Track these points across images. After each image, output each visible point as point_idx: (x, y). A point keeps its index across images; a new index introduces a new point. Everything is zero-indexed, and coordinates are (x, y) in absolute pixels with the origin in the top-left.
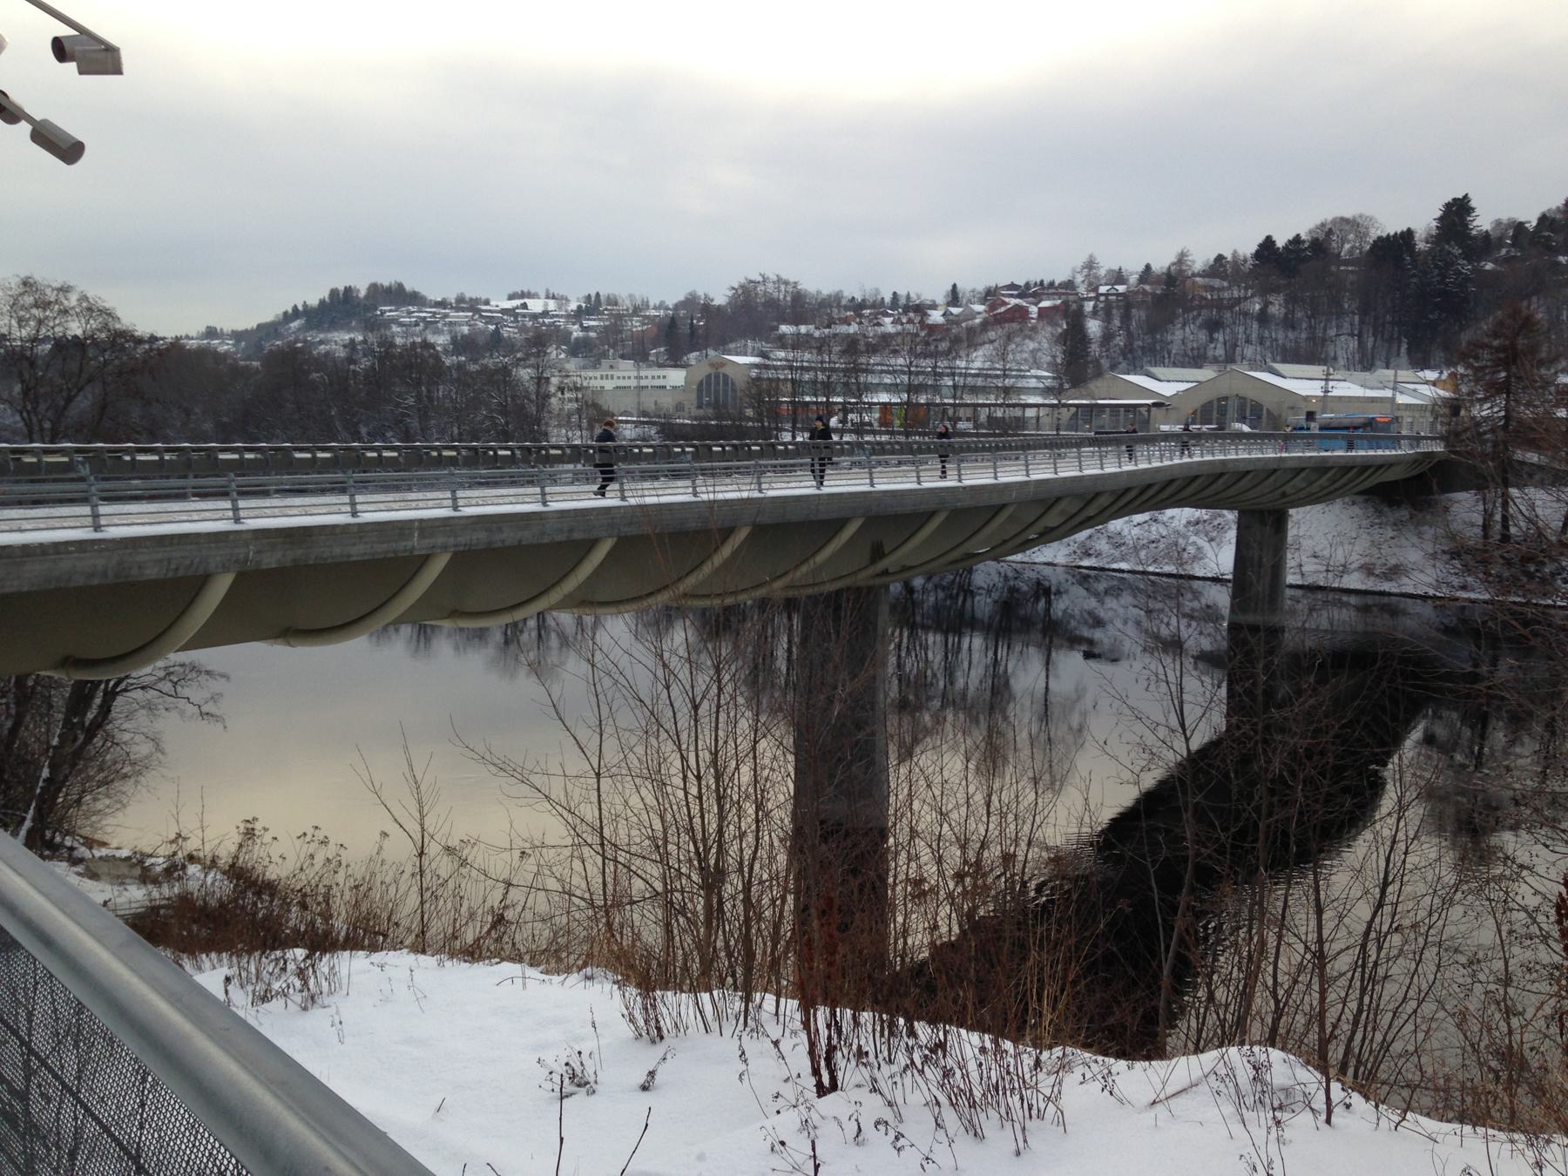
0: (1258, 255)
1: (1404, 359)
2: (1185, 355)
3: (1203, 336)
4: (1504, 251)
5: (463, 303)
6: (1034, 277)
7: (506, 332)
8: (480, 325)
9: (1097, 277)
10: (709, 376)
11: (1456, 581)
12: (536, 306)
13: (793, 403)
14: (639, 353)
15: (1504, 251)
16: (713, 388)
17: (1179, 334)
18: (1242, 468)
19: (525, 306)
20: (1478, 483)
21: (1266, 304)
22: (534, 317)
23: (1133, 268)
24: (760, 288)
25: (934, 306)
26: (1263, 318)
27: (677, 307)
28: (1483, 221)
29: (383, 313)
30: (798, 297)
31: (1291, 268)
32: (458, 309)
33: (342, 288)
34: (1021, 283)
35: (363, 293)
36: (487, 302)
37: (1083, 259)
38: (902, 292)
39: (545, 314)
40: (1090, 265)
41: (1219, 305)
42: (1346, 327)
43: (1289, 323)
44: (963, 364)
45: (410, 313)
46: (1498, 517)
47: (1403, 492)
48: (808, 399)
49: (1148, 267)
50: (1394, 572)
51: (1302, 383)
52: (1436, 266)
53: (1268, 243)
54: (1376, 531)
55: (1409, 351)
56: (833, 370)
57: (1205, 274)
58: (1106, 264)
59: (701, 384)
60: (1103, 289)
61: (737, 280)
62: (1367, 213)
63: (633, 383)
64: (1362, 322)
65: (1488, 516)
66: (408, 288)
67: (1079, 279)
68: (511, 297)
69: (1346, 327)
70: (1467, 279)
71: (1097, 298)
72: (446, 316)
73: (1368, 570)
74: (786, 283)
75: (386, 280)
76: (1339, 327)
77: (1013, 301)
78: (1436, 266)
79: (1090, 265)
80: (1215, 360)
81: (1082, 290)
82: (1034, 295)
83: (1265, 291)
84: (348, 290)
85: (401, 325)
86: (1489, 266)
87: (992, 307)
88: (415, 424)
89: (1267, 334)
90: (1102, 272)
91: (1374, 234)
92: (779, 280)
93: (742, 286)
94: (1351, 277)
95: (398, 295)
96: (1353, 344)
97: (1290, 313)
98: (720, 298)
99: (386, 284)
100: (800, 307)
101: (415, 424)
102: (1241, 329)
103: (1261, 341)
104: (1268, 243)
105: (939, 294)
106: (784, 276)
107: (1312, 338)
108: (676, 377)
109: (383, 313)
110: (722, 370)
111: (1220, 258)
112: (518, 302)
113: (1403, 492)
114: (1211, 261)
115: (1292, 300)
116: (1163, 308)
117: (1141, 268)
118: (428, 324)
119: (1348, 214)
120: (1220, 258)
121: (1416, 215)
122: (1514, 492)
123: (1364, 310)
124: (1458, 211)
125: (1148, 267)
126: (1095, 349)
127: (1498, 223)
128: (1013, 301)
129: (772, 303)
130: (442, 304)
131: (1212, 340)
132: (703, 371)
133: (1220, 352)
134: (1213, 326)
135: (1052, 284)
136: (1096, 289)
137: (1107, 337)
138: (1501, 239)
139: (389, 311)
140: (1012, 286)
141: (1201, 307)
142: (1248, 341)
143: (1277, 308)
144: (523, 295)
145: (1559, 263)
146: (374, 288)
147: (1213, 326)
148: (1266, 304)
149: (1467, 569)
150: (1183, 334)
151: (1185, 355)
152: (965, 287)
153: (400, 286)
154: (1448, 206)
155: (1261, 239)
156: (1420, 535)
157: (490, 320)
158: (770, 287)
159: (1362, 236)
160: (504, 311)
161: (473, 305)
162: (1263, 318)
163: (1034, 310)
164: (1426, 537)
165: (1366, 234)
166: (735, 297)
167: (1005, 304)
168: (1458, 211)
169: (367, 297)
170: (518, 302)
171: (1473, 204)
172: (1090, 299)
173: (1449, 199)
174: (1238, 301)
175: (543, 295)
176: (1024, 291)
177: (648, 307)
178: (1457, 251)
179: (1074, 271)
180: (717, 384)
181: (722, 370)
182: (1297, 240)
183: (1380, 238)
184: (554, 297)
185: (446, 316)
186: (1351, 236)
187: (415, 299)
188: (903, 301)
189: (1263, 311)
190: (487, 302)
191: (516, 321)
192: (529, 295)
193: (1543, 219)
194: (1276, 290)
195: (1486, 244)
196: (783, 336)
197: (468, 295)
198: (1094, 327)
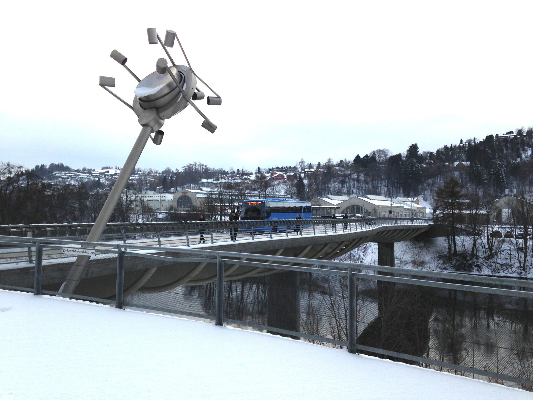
0: (355, 160)
1: (402, 194)
2: (335, 191)
3: (340, 186)
4: (427, 161)
5: (84, 171)
6: (284, 165)
7: (102, 181)
8: (92, 178)
9: (304, 166)
10: (182, 197)
11: (442, 266)
12: (112, 172)
13: (220, 206)
14: (153, 187)
15: (427, 161)
16: (184, 200)
17: (333, 185)
18: (401, 228)
19: (108, 172)
20: (447, 235)
21: (358, 176)
22: (112, 175)
23: (315, 163)
24: (194, 167)
25: (252, 174)
26: (358, 180)
27: (163, 172)
28: (421, 152)
29: (56, 174)
30: (207, 170)
31: (365, 164)
32: (84, 173)
33: (40, 165)
34: (280, 167)
35: (48, 167)
36: (94, 170)
37: (299, 161)
38: (241, 169)
39: (116, 174)
40: (302, 162)
41: (345, 176)
42: (383, 184)
43: (366, 182)
44: (278, 194)
45: (65, 174)
46: (453, 245)
47: (421, 237)
48: (226, 204)
49: (319, 163)
50: (422, 264)
51: (379, 201)
52: (410, 165)
53: (358, 157)
54: (414, 250)
55: (403, 192)
56: (234, 195)
57: (337, 165)
58: (307, 162)
59: (179, 199)
60: (306, 170)
61: (186, 164)
62: (387, 148)
63: (159, 199)
64: (388, 182)
65: (450, 246)
66: (65, 165)
67: (299, 166)
68: (103, 169)
69: (383, 184)
70: (419, 169)
71: (305, 172)
72: (79, 175)
73: (414, 263)
74: (203, 165)
75: (57, 163)
76: (381, 184)
77: (279, 173)
78: (410, 165)
79: (302, 162)
80: (345, 194)
81: (300, 169)
82: (285, 171)
83: (358, 172)
84: (42, 166)
85: (62, 178)
86: (425, 166)
87: (272, 175)
88: (77, 213)
89: (359, 185)
90: (306, 164)
91: (389, 155)
92: (200, 164)
93: (188, 166)
94: (384, 168)
95: (61, 168)
96: (386, 189)
97: (366, 179)
98: (181, 170)
99: (57, 164)
100: (208, 173)
101: (77, 213)
102: (351, 184)
103: (358, 187)
104: (358, 157)
105: (254, 170)
106: (202, 163)
107: (373, 187)
108: (169, 197)
109: (56, 174)
110: (186, 194)
111: (341, 161)
112: (106, 170)
113: (421, 237)
114: (339, 162)
115: (366, 175)
116: (327, 177)
117: (317, 163)
118: (72, 178)
119: (381, 149)
120: (341, 161)
121: (402, 150)
122: (457, 237)
123: (388, 178)
124: (414, 148)
125: (319, 163)
126: (307, 189)
127: (425, 152)
128: (279, 173)
129: (197, 171)
130: (78, 171)
131: (342, 187)
132: (179, 195)
133: (345, 191)
134: (343, 183)
135: (290, 168)
136: (304, 170)
137: (310, 185)
138: (426, 157)
139: (58, 173)
140: (278, 168)
141: (339, 176)
142: (354, 187)
143: (362, 177)
144: (107, 168)
145: (445, 165)
146: (52, 165)
147: (343, 183)
148: (358, 176)
149: (445, 263)
150: (334, 185)
151: (335, 191)
152: (262, 168)
153: (62, 165)
154: (411, 147)
155: (356, 156)
156: (428, 251)
157: (95, 177)
158: (197, 167)
159: (386, 155)
160: (100, 174)
161: (89, 171)
162: (358, 180)
163: (285, 176)
164: (430, 252)
165: (387, 155)
166: (186, 170)
167: (276, 174)
168: (414, 148)
169: (49, 168)
170: (106, 170)
171: (418, 146)
172: (302, 173)
173: (411, 145)
174: (350, 175)
175: (114, 168)
176: (281, 170)
177: (152, 173)
178: (416, 161)
179: (297, 164)
180: (185, 199)
181: (186, 194)
182: (367, 156)
183: (391, 156)
184: (118, 169)
185: (79, 175)
186: (383, 155)
187: (68, 169)
188: (241, 172)
189: (358, 178)
190: (94, 170)
191: (105, 177)
192: (109, 168)
193: (438, 151)
194: (361, 172)
195: (421, 159)
196: (203, 183)
197: (87, 168)
198: (306, 182)
